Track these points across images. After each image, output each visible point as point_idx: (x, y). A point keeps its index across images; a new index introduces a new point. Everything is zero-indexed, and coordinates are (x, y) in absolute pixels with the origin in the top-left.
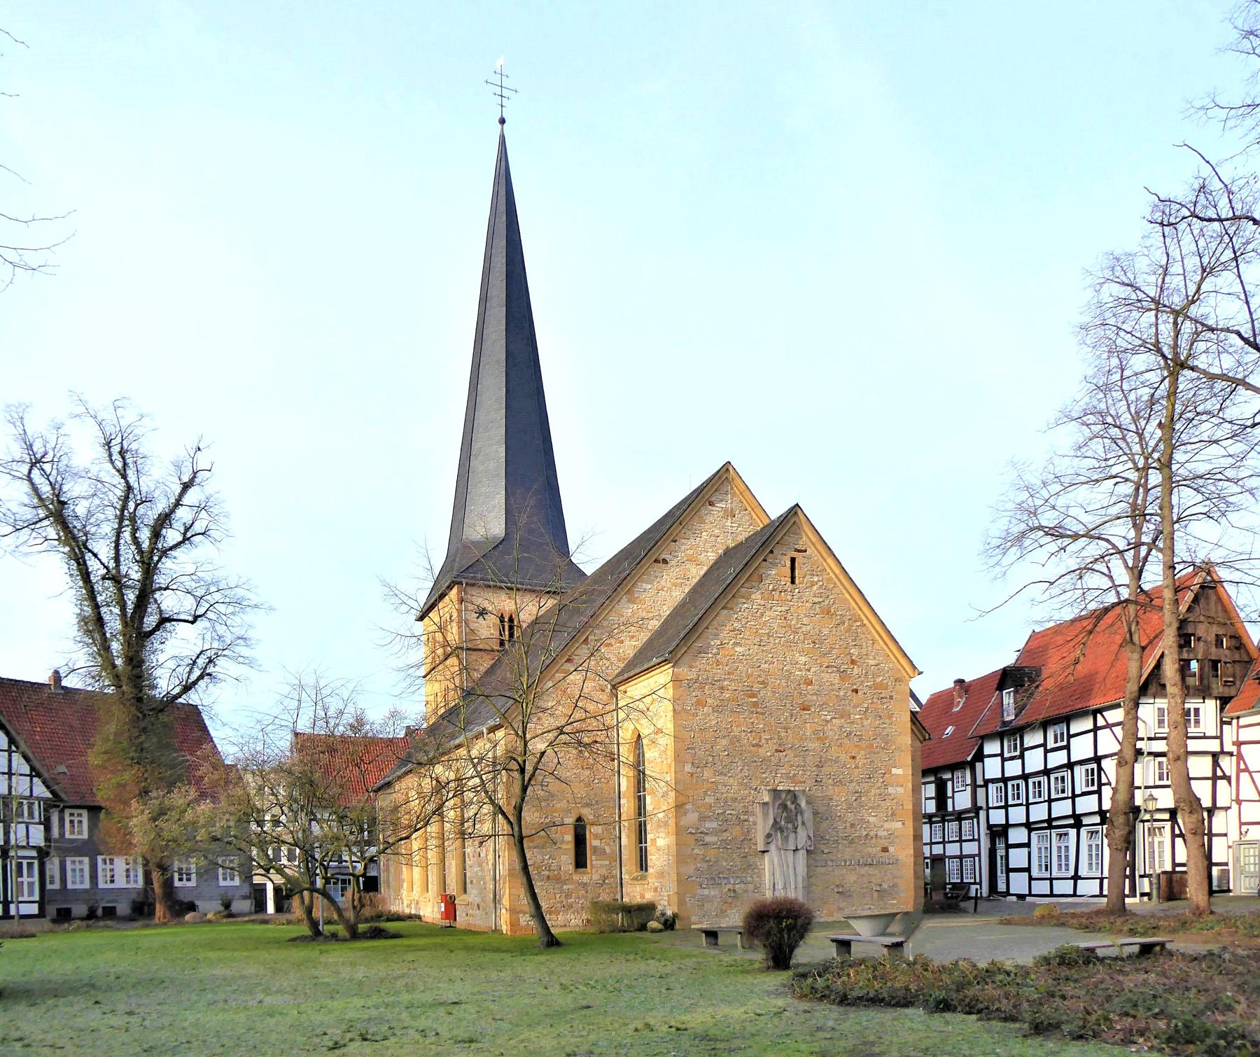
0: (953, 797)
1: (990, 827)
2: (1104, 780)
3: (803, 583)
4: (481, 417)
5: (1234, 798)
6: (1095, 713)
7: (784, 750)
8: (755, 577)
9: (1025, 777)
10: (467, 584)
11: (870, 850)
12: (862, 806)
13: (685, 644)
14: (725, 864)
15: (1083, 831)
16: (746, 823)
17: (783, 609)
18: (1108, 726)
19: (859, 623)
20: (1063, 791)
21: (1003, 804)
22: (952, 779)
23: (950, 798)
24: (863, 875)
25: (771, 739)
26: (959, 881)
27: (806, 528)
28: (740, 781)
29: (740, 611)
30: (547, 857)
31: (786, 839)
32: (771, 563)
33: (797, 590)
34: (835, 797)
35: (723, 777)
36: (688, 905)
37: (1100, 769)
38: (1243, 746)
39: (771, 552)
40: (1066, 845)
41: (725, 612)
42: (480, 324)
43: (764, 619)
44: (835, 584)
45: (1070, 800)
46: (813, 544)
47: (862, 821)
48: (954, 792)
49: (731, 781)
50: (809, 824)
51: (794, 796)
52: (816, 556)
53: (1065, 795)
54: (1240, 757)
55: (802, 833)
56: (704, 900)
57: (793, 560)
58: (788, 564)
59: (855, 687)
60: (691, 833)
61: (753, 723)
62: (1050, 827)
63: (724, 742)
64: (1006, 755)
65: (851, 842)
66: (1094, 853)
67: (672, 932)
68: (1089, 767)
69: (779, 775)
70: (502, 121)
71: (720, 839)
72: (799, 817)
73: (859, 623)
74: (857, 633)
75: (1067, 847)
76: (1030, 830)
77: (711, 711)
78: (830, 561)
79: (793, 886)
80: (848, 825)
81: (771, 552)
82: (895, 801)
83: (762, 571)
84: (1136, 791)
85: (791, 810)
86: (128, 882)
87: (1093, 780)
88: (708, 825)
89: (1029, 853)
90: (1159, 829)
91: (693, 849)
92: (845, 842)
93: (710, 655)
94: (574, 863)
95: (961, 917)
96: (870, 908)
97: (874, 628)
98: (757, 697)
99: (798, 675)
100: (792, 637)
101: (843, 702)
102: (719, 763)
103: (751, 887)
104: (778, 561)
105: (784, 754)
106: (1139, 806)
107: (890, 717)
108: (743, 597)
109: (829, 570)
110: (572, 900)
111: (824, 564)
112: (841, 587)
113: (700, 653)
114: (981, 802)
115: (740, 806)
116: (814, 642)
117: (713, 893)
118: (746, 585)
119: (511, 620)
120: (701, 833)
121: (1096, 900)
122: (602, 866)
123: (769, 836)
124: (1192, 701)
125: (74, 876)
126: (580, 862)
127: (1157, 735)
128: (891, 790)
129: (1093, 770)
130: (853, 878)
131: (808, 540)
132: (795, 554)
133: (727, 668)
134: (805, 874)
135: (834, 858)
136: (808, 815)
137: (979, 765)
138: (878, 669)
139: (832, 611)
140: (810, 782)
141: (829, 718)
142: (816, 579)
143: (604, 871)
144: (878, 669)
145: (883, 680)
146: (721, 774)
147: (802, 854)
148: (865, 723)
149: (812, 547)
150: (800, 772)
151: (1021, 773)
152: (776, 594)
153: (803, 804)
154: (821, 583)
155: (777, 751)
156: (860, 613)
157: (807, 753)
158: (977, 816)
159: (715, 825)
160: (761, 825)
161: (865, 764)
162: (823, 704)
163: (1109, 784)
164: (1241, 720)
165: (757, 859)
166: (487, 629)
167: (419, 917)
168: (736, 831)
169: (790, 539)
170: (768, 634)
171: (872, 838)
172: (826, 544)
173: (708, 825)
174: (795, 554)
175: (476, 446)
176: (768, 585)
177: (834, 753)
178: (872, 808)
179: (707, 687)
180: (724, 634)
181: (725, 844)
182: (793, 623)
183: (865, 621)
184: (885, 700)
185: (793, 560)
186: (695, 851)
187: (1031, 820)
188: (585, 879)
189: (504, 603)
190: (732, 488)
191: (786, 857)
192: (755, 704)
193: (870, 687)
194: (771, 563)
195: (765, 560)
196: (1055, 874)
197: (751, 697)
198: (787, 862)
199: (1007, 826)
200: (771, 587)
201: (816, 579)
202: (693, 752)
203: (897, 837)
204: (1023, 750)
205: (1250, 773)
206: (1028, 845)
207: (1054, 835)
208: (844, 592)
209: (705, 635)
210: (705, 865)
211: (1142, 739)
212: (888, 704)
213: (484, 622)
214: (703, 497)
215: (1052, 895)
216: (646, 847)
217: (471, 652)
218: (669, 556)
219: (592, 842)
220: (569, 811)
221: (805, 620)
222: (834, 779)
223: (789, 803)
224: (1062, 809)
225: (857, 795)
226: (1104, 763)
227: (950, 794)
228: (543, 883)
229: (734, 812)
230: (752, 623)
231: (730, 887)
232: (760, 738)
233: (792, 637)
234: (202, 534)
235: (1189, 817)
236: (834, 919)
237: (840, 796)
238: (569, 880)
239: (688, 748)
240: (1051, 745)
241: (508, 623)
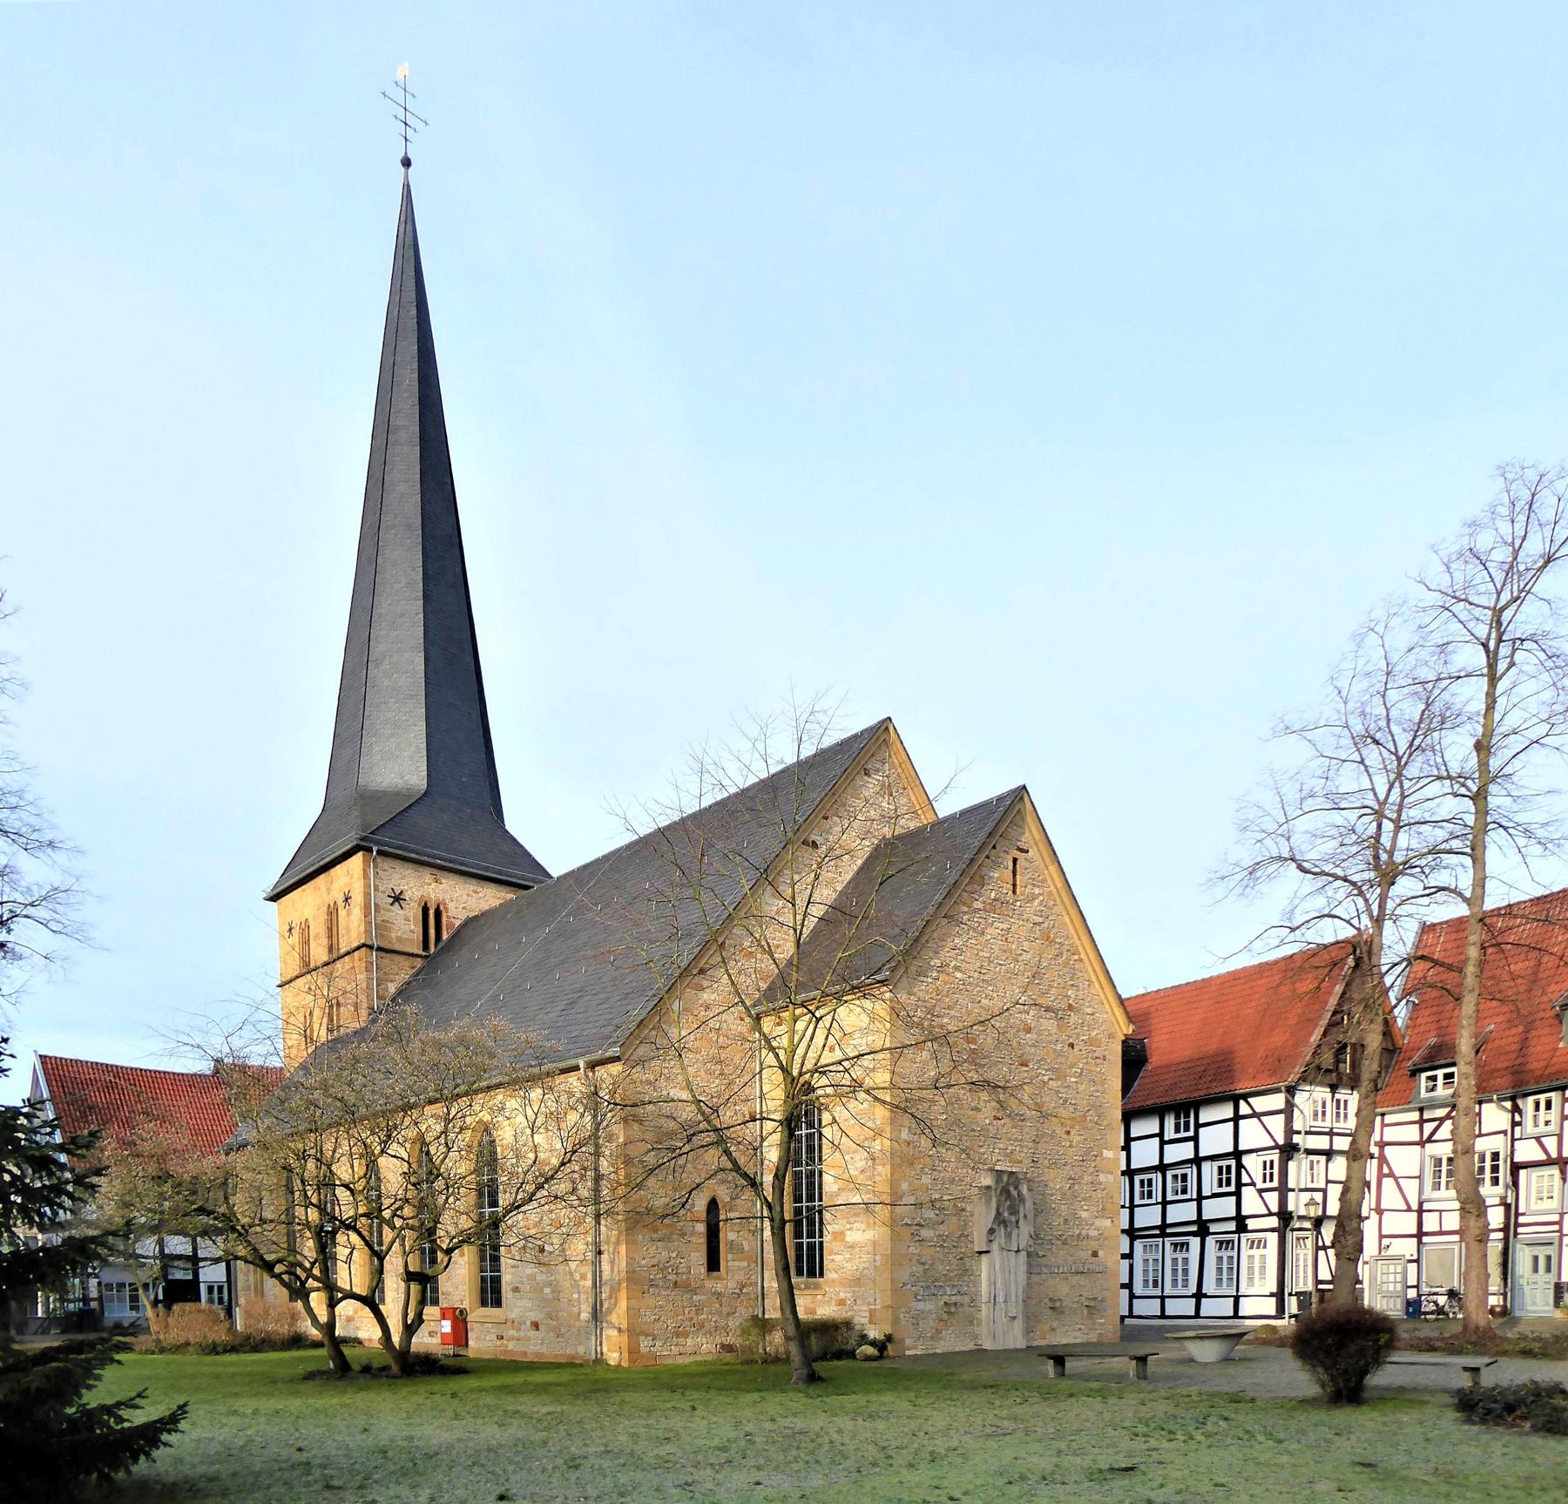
2: (1245, 1179)
4: (384, 605)
5: (1373, 1206)
6: (1236, 1099)
10: (380, 853)
12: (1076, 1197)
14: (941, 1268)
15: (1210, 1241)
18: (1255, 1115)
19: (1076, 957)
20: (1184, 1191)
27: (1030, 819)
30: (674, 1255)
31: (1009, 1236)
34: (1051, 1184)
36: (903, 1323)
37: (1240, 1166)
38: (1387, 1148)
39: (994, 847)
40: (1185, 1256)
45: (1160, 1206)
52: (1039, 862)
53: (1187, 1197)
54: (1383, 1160)
56: (917, 1318)
59: (1071, 1041)
60: (906, 1224)
62: (1163, 1235)
66: (1225, 1266)
68: (1224, 1163)
69: (997, 1151)
71: (937, 1233)
73: (1076, 957)
75: (1186, 1260)
76: (1133, 1239)
78: (1053, 868)
80: (1062, 1220)
83: (984, 871)
84: (1290, 1194)
87: (1272, 1174)
89: (1131, 1267)
90: (1304, 1239)
91: (909, 1247)
92: (1059, 1242)
93: (930, 980)
94: (706, 1265)
100: (1012, 965)
103: (967, 1299)
104: (1000, 860)
106: (1291, 1213)
109: (1049, 882)
110: (704, 1316)
111: (1046, 872)
121: (1230, 1322)
122: (740, 1269)
123: (991, 1231)
124: (1343, 1091)
126: (713, 1264)
127: (1313, 1129)
128: (1102, 1178)
129: (1229, 1168)
132: (1017, 854)
134: (1024, 1283)
138: (1093, 1019)
142: (1037, 891)
143: (741, 1277)
144: (1093, 1019)
145: (1097, 1034)
147: (1023, 1254)
148: (1081, 1088)
151: (1157, 1163)
154: (1041, 898)
160: (982, 1215)
161: (1079, 1142)
162: (1040, 1061)
163: (1253, 1184)
164: (1386, 1117)
166: (405, 927)
167: (359, 1342)
170: (989, 958)
172: (1051, 845)
175: (378, 649)
178: (1084, 1199)
182: (1014, 947)
184: (1099, 1061)
187: (1137, 1226)
189: (420, 886)
190: (890, 756)
195: (987, 857)
196: (1168, 1292)
198: (1009, 1266)
200: (993, 895)
201: (1037, 891)
203: (1106, 1238)
205: (1396, 1179)
210: (921, 1268)
211: (1299, 1133)
213: (401, 912)
214: (859, 762)
215: (1163, 1316)
216: (821, 1243)
217: (384, 954)
218: (819, 838)
219: (728, 1235)
221: (1026, 945)
224: (1182, 1213)
225: (1071, 1181)
226: (1246, 1160)
228: (668, 1292)
230: (974, 941)
235: (1477, 1221)
237: (1056, 1181)
240: (1170, 1133)
241: (431, 916)
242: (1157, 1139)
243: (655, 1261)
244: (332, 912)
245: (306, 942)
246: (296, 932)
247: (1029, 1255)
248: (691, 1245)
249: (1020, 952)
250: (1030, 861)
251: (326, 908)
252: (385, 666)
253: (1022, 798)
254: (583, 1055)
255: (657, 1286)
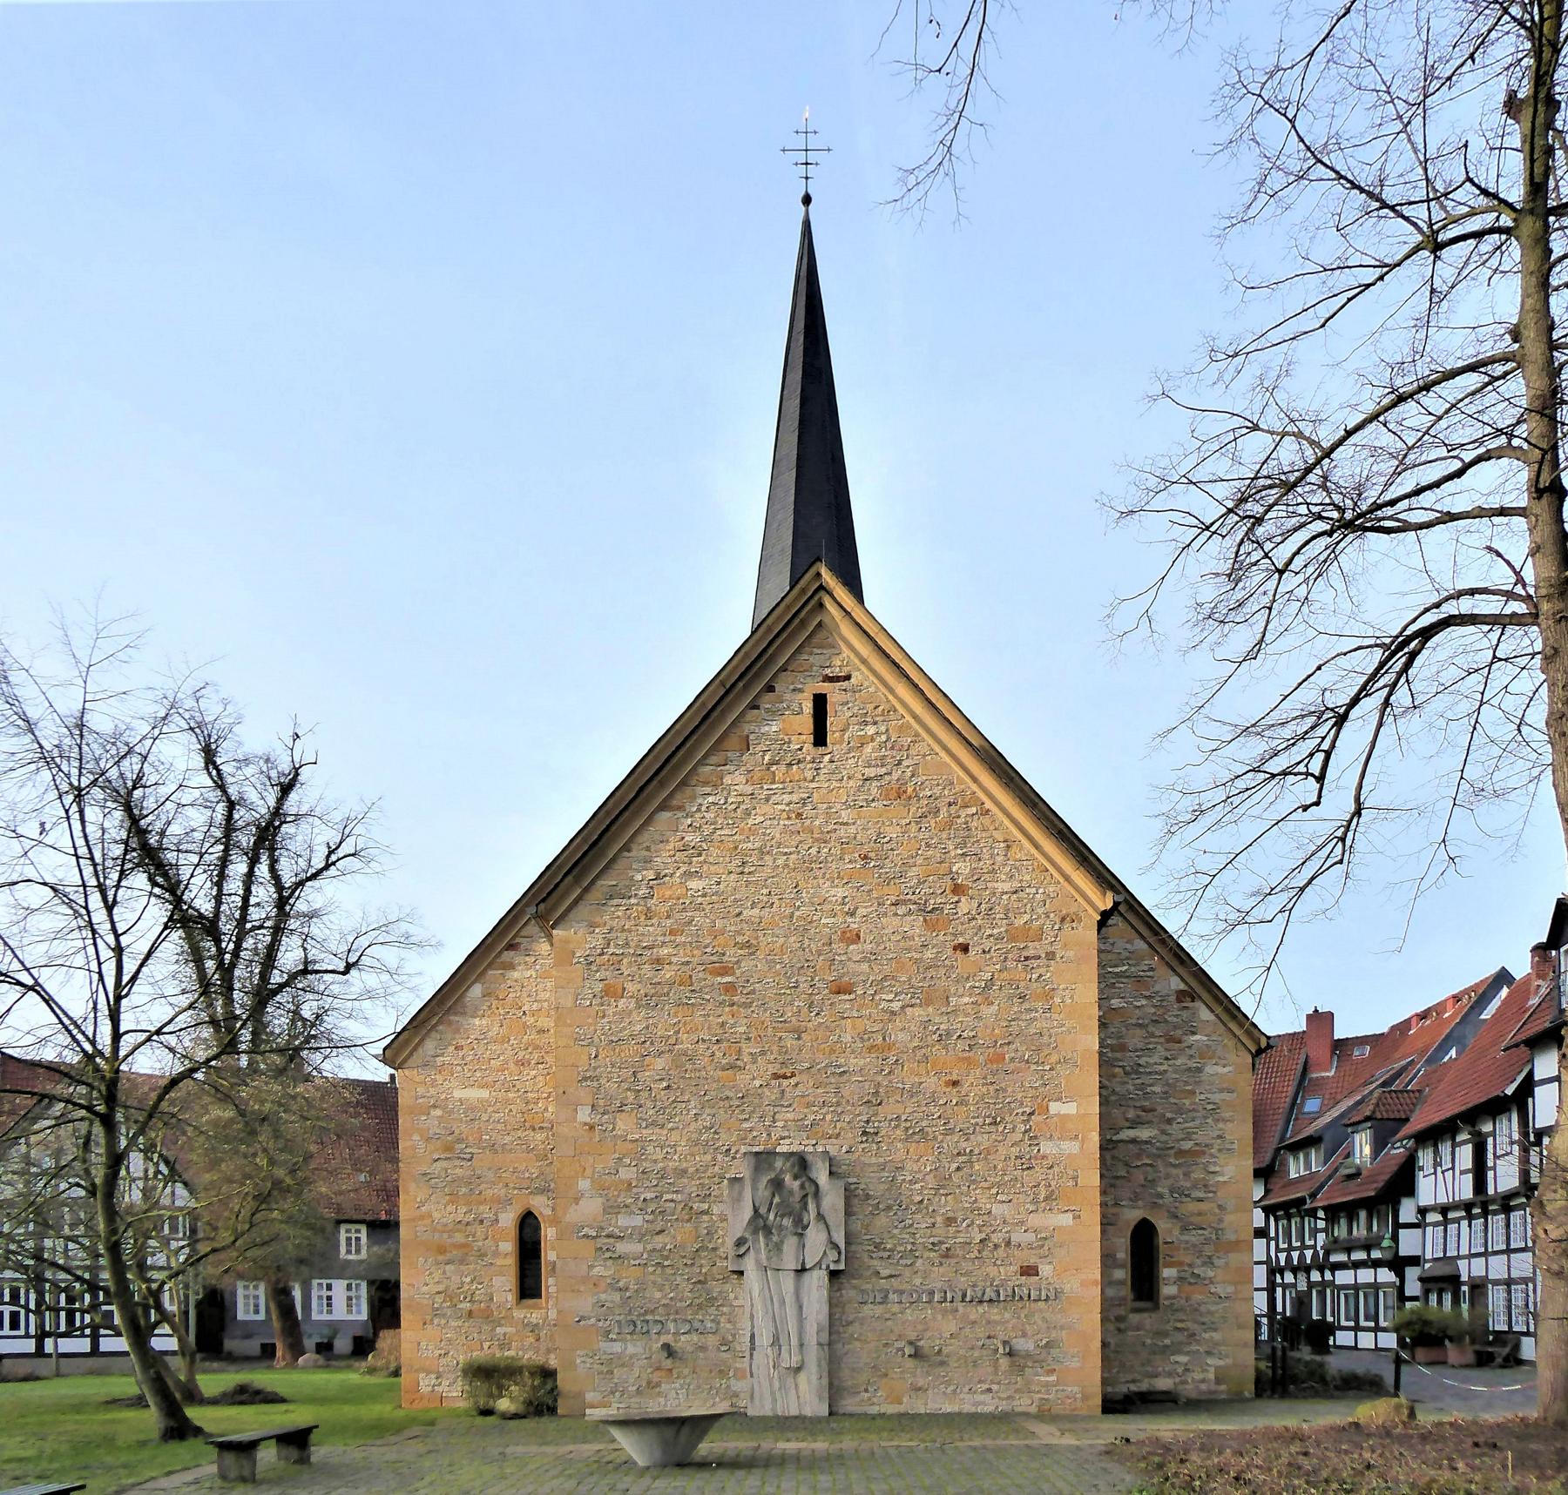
0: (1494, 1168)
3: (841, 742)
7: (793, 1075)
8: (733, 741)
11: (993, 1271)
13: (577, 880)
16: (705, 1218)
17: (795, 798)
22: (1493, 1133)
23: (1491, 1169)
24: (974, 1322)
25: (763, 1053)
26: (1506, 1328)
28: (694, 1136)
29: (699, 810)
30: (468, 1279)
32: (768, 711)
33: (827, 758)
35: (657, 1130)
39: (770, 688)
41: (665, 815)
43: (751, 822)
44: (917, 735)
46: (864, 661)
47: (975, 1209)
48: (1496, 1157)
49: (675, 1136)
50: (836, 1218)
51: (802, 1164)
55: (815, 1238)
56: (610, 1365)
57: (820, 702)
58: (808, 707)
59: (961, 940)
61: (723, 1024)
63: (660, 1063)
65: (947, 1254)
67: (553, 1418)
70: (807, 200)
71: (649, 1247)
72: (811, 1206)
74: (969, 829)
77: (632, 1005)
79: (794, 1341)
80: (939, 1219)
81: (770, 688)
82: (1056, 1169)
83: (747, 728)
85: (791, 1193)
86: (350, 1312)
88: (623, 1221)
92: (932, 1254)
95: (1148, 1417)
96: (989, 1390)
97: (1008, 815)
98: (733, 974)
99: (826, 925)
100: (813, 851)
101: (932, 972)
102: (649, 1104)
105: (793, 1081)
107: (1049, 995)
108: (706, 783)
109: (901, 710)
111: (891, 697)
112: (930, 741)
113: (611, 898)
115: (692, 1188)
116: (866, 857)
117: (631, 1349)
118: (713, 759)
120: (608, 1236)
123: (740, 1242)
125: (247, 1305)
126: (529, 1287)
128: (1047, 1147)
130: (950, 1326)
131: (852, 656)
132: (825, 688)
133: (669, 922)
135: (905, 1287)
136: (832, 1199)
139: (910, 790)
140: (851, 1137)
141: (896, 1006)
146: (654, 1124)
147: (818, 1279)
149: (863, 668)
150: (828, 1117)
152: (779, 770)
153: (822, 1177)
154: (884, 738)
155: (776, 1076)
156: (974, 787)
157: (845, 1077)
159: (638, 1221)
165: (728, 1287)
168: (682, 1234)
169: (813, 659)
171: (996, 1246)
173: (623, 1221)
174: (825, 688)
176: (758, 755)
177: (907, 1076)
179: (625, 961)
180: (664, 858)
181: (661, 1259)
182: (817, 823)
183: (989, 805)
184: (1035, 963)
185: (820, 702)
186: (596, 1271)
188: (535, 1316)
191: (778, 1282)
192: (730, 988)
193: (999, 938)
194: (768, 711)
197: (722, 975)
199: (1316, 1218)
201: (871, 730)
202: (595, 1084)
208: (937, 748)
209: (620, 865)
210: (617, 1297)
212: (1042, 971)
220: (509, 1202)
221: (845, 816)
222: (907, 1129)
223: (788, 1178)
225: (961, 1159)
227: (1490, 1164)
228: (460, 1323)
229: (679, 1197)
231: (665, 1339)
232: (739, 1051)
233: (813, 851)
234: (352, 855)
236: (901, 1409)
238: (508, 1318)
239: (585, 1079)
243: (441, 1288)
248: (493, 1268)
249: (831, 827)
253: (821, 605)
255: (444, 1315)
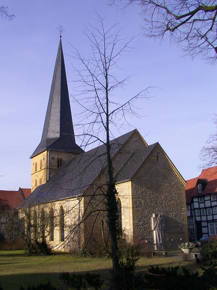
1: (196, 221)
4: (54, 105)
9: (206, 208)
21: (200, 215)
42: (53, 83)
57: (157, 155)
64: (200, 202)
70: (61, 37)
73: (173, 171)
80: (173, 223)
114: (193, 214)
119: (61, 160)
132: (157, 154)
137: (192, 204)
158: (192, 218)
174: (157, 154)
185: (157, 155)
199: (201, 221)
201: (162, 160)
204: (205, 201)
206: (207, 227)
207: (215, 225)
213: (54, 161)
240: (212, 200)
242: (210, 201)
244: (41, 161)
245: (36, 167)
246: (35, 164)
247: (164, 230)
250: (160, 155)
251: (40, 160)
252: (53, 116)
254: (77, 194)
